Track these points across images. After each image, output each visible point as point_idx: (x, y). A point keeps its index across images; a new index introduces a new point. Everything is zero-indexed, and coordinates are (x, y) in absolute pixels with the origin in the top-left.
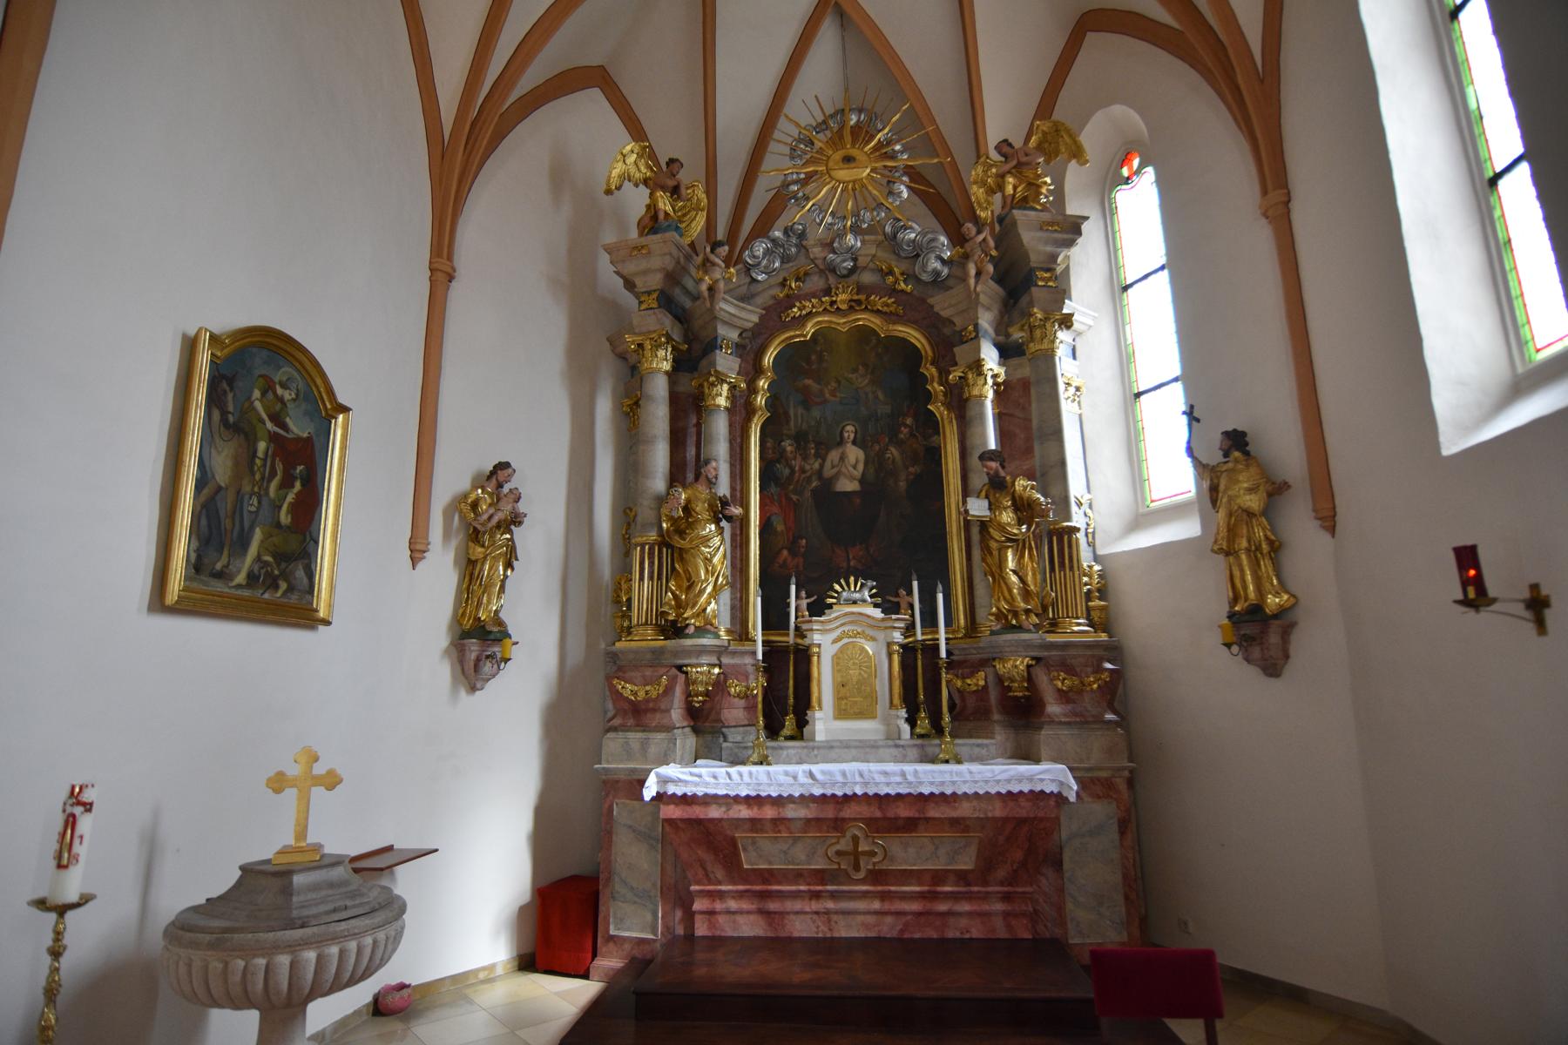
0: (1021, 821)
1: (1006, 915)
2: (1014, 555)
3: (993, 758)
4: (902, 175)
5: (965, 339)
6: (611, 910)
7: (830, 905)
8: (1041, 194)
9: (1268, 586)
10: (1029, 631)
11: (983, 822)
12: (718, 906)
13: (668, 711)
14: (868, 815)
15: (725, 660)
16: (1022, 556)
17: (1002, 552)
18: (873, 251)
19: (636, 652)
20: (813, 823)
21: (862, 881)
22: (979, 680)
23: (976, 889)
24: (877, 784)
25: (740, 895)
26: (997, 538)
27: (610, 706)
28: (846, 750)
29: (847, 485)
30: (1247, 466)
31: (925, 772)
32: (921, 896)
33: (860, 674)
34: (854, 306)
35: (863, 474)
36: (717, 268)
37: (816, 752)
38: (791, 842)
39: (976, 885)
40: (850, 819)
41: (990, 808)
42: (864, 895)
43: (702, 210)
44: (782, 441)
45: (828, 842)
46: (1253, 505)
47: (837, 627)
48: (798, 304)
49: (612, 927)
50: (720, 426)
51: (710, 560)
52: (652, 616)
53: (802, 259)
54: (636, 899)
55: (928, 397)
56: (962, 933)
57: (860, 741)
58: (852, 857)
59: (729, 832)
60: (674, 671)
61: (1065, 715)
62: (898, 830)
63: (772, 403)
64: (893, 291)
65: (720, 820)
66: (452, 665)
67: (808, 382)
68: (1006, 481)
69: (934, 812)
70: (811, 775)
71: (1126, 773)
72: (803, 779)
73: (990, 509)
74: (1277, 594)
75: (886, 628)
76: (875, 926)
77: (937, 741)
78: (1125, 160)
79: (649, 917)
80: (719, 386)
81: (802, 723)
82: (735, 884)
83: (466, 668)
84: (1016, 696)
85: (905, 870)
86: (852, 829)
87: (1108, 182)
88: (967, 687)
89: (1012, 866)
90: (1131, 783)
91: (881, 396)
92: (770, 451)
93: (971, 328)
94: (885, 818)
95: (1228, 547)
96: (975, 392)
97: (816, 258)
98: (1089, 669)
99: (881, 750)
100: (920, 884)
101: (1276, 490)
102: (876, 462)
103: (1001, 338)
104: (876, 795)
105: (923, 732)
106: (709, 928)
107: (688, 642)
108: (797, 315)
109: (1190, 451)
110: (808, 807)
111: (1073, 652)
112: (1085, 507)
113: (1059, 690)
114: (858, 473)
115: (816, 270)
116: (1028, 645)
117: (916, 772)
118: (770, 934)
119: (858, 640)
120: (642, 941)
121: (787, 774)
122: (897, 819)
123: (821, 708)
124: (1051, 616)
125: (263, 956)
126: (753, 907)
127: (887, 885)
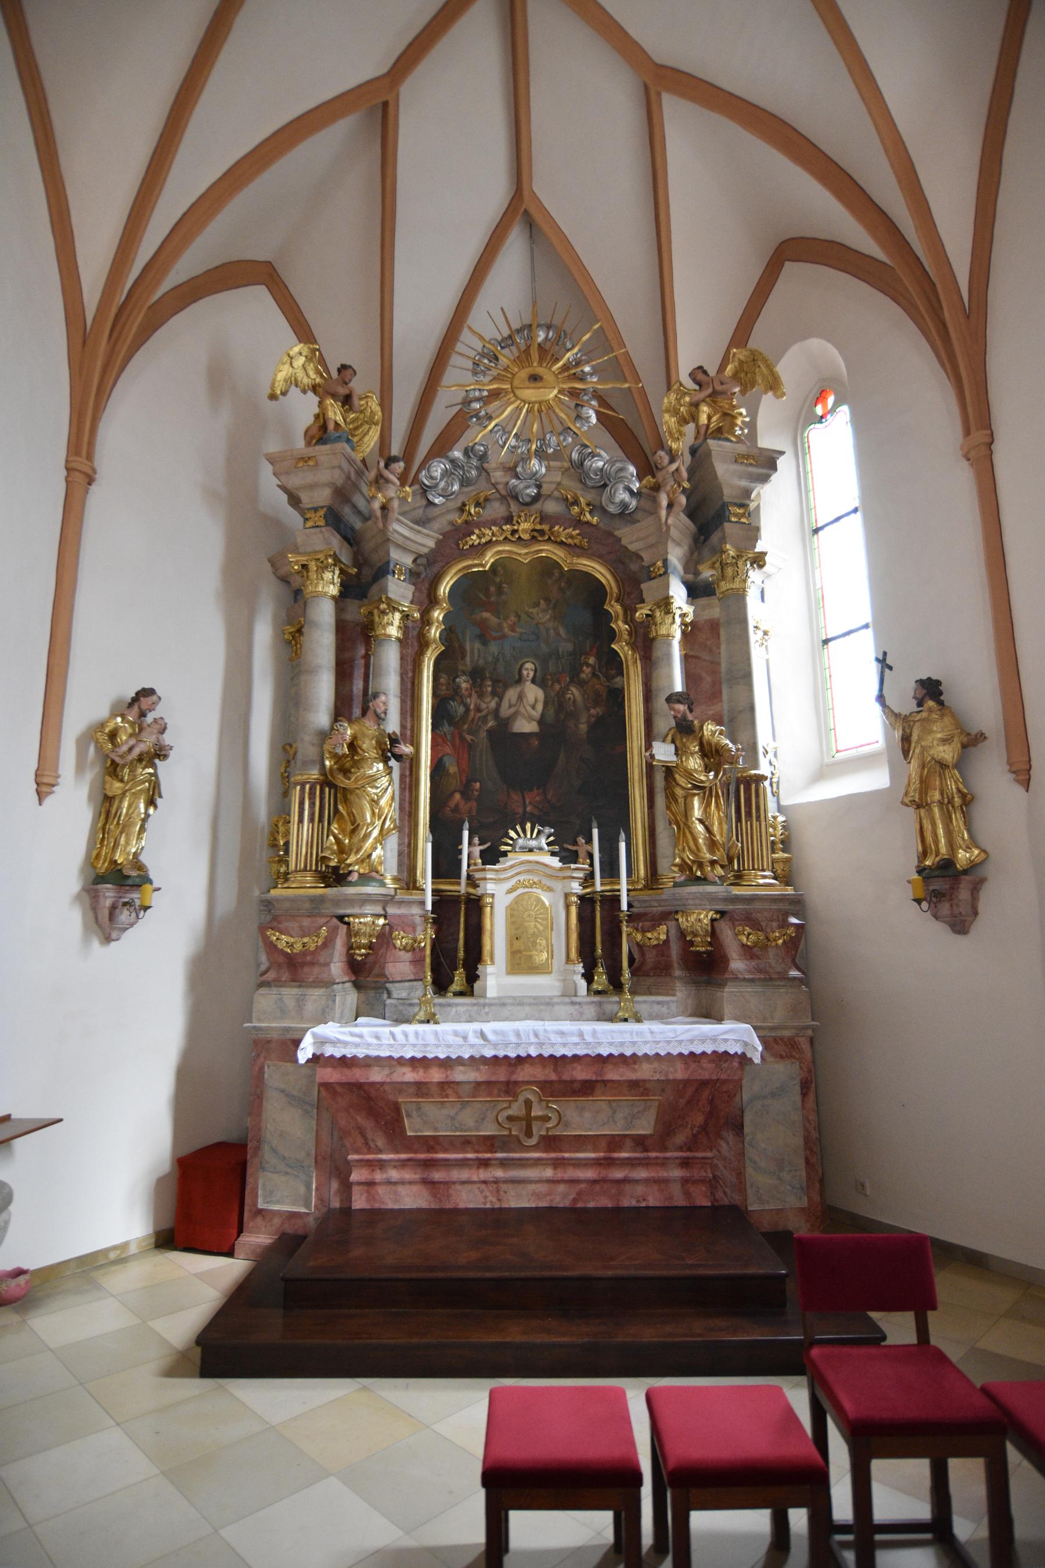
0: (704, 1083)
1: (685, 1181)
2: (701, 803)
4: (591, 399)
7: (499, 1173)
8: (737, 425)
10: (714, 883)
12: (378, 1176)
13: (327, 965)
15: (391, 910)
16: (708, 805)
17: (688, 801)
19: (293, 900)
22: (661, 934)
23: (653, 1155)
24: (553, 1045)
25: (403, 1164)
26: (683, 785)
27: (263, 958)
29: (525, 726)
30: (942, 716)
31: (604, 1032)
32: (597, 1163)
34: (536, 536)
35: (543, 715)
37: (487, 1009)
38: (459, 1106)
40: (523, 1082)
42: (537, 1163)
43: (376, 424)
44: (457, 677)
46: (947, 756)
47: (512, 876)
48: (477, 531)
49: (260, 1200)
50: (390, 658)
51: (377, 802)
52: (311, 861)
53: (482, 484)
54: (289, 1170)
55: (612, 635)
56: (638, 1201)
57: (535, 998)
58: (524, 1123)
59: (391, 1097)
60: (335, 921)
61: (749, 972)
62: (575, 1093)
63: (449, 635)
64: (578, 523)
65: (382, 1084)
67: (486, 615)
69: (612, 1074)
70: (482, 1035)
72: (473, 1039)
73: (676, 754)
75: (564, 878)
76: (546, 1195)
77: (616, 999)
78: (821, 398)
79: (302, 1190)
80: (390, 615)
81: (472, 977)
82: (398, 1152)
84: (698, 952)
85: (581, 1136)
86: (524, 1093)
87: (801, 420)
88: (647, 941)
89: (692, 1129)
91: (562, 631)
92: (444, 688)
93: (660, 563)
94: (561, 1081)
95: (921, 799)
96: (663, 631)
97: (497, 483)
99: (557, 1008)
102: (556, 703)
104: (552, 1056)
105: (600, 988)
106: (368, 1200)
107: (351, 890)
109: (881, 698)
110: (478, 1070)
111: (758, 905)
112: (770, 756)
113: (743, 945)
114: (537, 713)
116: (712, 898)
117: (594, 1032)
118: (437, 1206)
119: (534, 890)
120: (293, 1215)
121: (456, 1033)
122: (573, 1082)
124: (736, 867)
126: (417, 1177)
127: (561, 1151)
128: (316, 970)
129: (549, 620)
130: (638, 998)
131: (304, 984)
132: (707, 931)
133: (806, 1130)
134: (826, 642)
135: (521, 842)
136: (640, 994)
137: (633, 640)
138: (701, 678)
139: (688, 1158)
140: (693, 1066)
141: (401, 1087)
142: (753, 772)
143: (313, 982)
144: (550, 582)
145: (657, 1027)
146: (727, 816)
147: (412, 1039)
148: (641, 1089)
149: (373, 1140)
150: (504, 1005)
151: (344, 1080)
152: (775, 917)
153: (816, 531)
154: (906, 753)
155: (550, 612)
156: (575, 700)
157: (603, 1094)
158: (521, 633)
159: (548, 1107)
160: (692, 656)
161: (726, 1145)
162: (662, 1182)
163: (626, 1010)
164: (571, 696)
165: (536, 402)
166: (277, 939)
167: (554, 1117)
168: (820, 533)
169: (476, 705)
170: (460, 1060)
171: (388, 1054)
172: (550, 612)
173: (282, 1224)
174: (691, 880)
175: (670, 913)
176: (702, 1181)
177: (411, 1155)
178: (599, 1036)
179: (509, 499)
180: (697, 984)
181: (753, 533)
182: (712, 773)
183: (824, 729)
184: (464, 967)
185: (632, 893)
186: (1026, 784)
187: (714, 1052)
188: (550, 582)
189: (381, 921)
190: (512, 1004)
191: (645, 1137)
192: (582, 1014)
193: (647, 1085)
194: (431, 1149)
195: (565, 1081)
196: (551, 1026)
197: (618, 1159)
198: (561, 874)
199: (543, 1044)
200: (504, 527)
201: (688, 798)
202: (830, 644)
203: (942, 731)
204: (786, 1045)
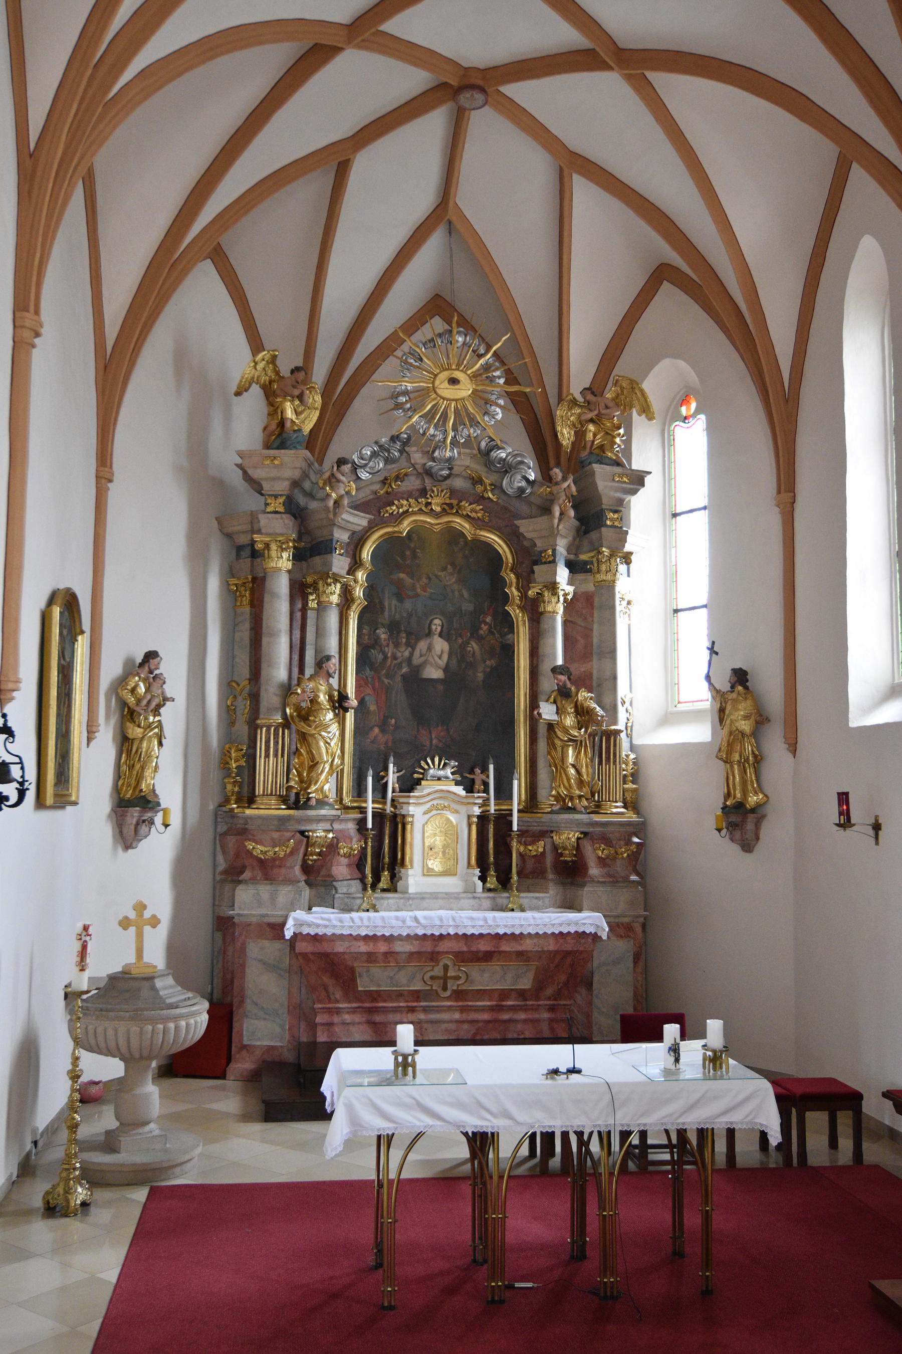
0: (568, 953)
1: (551, 1020)
2: (574, 752)
3: (547, 908)
4: (498, 398)
5: (544, 560)
6: (245, 1026)
7: (422, 1016)
8: (615, 443)
9: (750, 787)
10: (581, 813)
11: (540, 955)
12: (336, 1019)
13: (292, 867)
14: (457, 950)
15: (336, 826)
16: (579, 753)
17: (564, 750)
18: (467, 463)
20: (415, 956)
21: (448, 999)
22: (540, 846)
23: (530, 1003)
24: (465, 926)
25: (353, 1011)
26: (562, 738)
28: (435, 901)
29: (434, 673)
30: (746, 699)
31: (501, 918)
32: (491, 1009)
33: (445, 839)
36: (341, 484)
37: (411, 902)
38: (397, 969)
39: (531, 1000)
40: (443, 952)
41: (546, 944)
42: (449, 1008)
43: (316, 409)
44: (376, 629)
45: (425, 970)
46: (746, 728)
47: (429, 801)
48: (396, 502)
49: (245, 1038)
52: (276, 788)
53: (403, 462)
54: (267, 1017)
55: (506, 599)
56: (518, 1035)
57: (446, 894)
58: (442, 981)
59: (349, 963)
60: (298, 835)
61: (603, 876)
62: (479, 960)
63: (370, 591)
64: (480, 499)
65: (344, 953)
66: (113, 828)
68: (571, 692)
69: (505, 947)
70: (416, 919)
71: (642, 919)
73: (557, 713)
74: (756, 793)
75: (469, 803)
76: (455, 1031)
77: (506, 895)
78: (684, 401)
80: (333, 585)
81: (393, 877)
82: (350, 1002)
83: (125, 831)
84: (566, 861)
85: (481, 990)
86: (443, 960)
87: (668, 418)
88: (528, 852)
89: (558, 985)
90: (644, 926)
91: (465, 594)
92: (366, 637)
93: (550, 552)
94: (470, 952)
95: (727, 758)
96: (549, 608)
97: (417, 464)
98: (622, 842)
99: (462, 901)
100: (490, 1000)
101: (761, 720)
102: (459, 654)
103: (572, 557)
104: (465, 935)
105: (492, 887)
106: (328, 1037)
108: (395, 513)
109: (708, 678)
110: (412, 944)
111: (611, 829)
112: (627, 705)
113: (599, 858)
114: (443, 662)
115: (415, 472)
116: (579, 823)
117: (494, 918)
119: (444, 812)
121: (397, 918)
122: (478, 952)
123: (412, 867)
124: (596, 798)
125: (161, 1023)
127: (466, 1000)
128: (283, 871)
129: (455, 583)
130: (522, 895)
131: (274, 882)
132: (573, 846)
133: (635, 987)
134: (676, 611)
135: (431, 771)
136: (524, 891)
137: (523, 604)
138: (577, 641)
139: (554, 1005)
140: (561, 941)
141: (357, 956)
142: (613, 727)
143: (283, 880)
144: (456, 549)
145: (537, 915)
146: (592, 760)
147: (366, 923)
148: (525, 958)
149: (333, 994)
150: (423, 898)
151: (316, 950)
152: (623, 837)
153: (675, 515)
154: (721, 720)
155: (455, 575)
156: (474, 653)
157: (499, 961)
158: (432, 593)
159: (459, 970)
160: (570, 621)
161: (580, 998)
162: (537, 1021)
163: (514, 903)
164: (471, 649)
165: (453, 400)
166: (253, 848)
167: (463, 976)
168: (678, 518)
169: (393, 653)
170: (400, 938)
171: (348, 933)
172: (455, 575)
173: (263, 1054)
174: (563, 809)
175: (546, 832)
176: (563, 1021)
177: (360, 1005)
178: (498, 920)
179: (424, 475)
180: (563, 884)
181: (622, 535)
182: (583, 730)
183: (671, 683)
184: (388, 870)
185: (50, 800)
186: (794, 752)
187: (576, 932)
188: (456, 549)
189: (331, 835)
190: (429, 898)
191: (524, 990)
192: (480, 905)
193: (529, 955)
194: (375, 1000)
195: (473, 952)
196: (465, 914)
197: (506, 1006)
198: (465, 801)
199: (459, 926)
200: (420, 500)
201: (564, 748)
202: (679, 614)
203: (745, 709)
204: (625, 928)
